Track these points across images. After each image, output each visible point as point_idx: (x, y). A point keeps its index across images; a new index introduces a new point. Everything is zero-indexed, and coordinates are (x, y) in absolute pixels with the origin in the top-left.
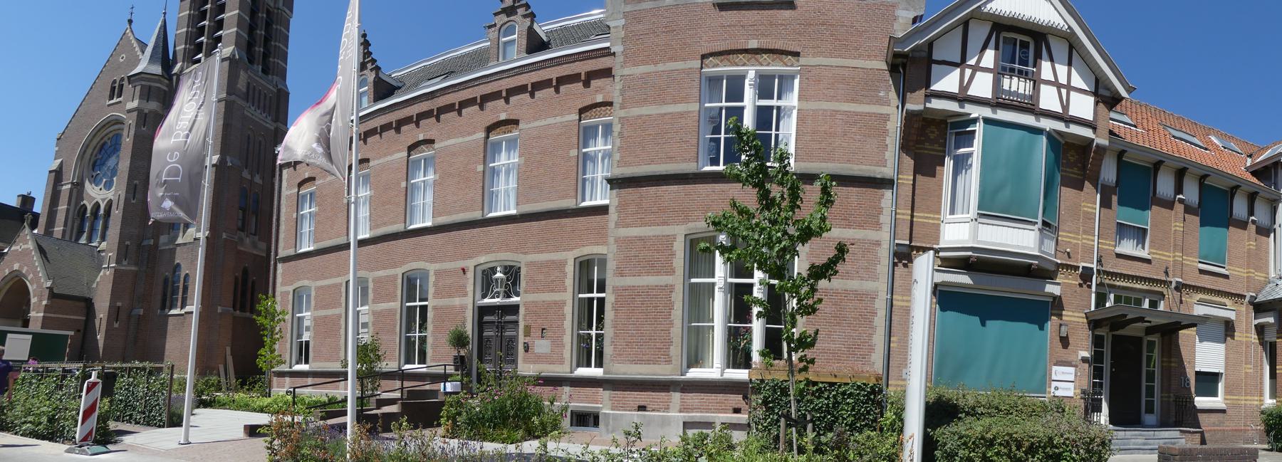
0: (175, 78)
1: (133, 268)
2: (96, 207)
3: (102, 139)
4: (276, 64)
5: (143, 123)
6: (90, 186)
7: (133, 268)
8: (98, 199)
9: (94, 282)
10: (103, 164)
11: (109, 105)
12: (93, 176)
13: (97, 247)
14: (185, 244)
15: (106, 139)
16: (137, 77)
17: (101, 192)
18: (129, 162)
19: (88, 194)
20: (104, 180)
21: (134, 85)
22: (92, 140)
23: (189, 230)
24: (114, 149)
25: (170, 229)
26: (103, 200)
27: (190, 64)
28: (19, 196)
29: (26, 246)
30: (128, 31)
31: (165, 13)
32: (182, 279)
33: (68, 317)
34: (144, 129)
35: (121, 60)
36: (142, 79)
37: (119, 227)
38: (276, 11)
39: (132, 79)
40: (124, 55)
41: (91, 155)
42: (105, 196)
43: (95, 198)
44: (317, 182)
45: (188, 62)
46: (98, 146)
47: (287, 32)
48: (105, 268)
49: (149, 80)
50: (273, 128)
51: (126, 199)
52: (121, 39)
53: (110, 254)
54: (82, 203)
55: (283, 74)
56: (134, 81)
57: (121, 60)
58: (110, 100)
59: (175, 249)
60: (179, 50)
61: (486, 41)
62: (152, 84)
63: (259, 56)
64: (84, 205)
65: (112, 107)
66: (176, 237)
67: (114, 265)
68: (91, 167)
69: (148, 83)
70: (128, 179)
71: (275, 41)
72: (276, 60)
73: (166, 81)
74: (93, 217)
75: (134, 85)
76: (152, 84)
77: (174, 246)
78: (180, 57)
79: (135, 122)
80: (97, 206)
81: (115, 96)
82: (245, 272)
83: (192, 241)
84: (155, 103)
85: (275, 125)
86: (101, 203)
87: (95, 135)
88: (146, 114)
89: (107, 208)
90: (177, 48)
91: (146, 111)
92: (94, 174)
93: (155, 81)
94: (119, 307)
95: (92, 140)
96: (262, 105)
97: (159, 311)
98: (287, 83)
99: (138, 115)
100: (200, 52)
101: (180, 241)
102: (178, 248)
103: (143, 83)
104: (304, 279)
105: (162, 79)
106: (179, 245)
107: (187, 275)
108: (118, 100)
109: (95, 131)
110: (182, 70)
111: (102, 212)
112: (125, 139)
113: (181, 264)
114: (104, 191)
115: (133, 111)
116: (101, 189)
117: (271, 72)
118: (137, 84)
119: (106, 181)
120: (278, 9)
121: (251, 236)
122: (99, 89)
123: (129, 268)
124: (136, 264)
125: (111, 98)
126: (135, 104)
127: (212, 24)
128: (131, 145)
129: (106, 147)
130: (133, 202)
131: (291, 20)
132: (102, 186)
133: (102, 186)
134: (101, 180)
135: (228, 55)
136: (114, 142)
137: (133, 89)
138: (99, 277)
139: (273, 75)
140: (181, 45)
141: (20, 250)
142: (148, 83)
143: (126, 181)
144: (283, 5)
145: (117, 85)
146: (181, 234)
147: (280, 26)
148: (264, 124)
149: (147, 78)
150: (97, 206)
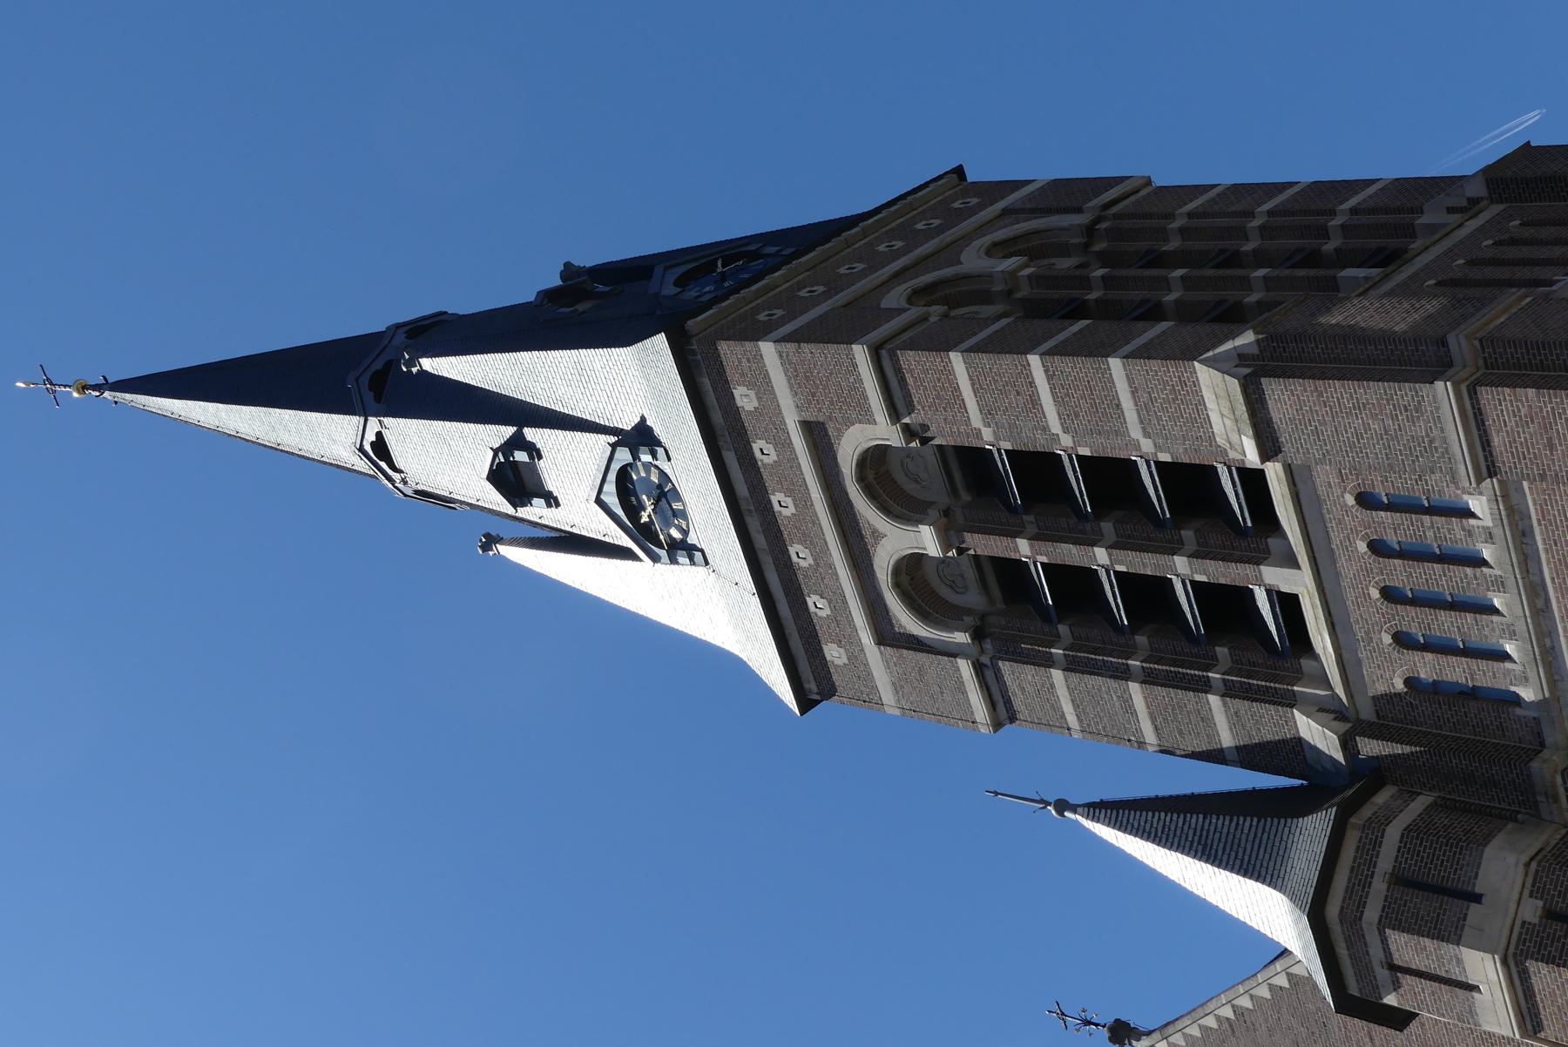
0: (1370, 747)
16: (1342, 951)
21: (1382, 974)
69: (1379, 886)
71: (1324, 234)
75: (1382, 974)
76: (1385, 863)
78: (1266, 724)
84: (1489, 851)
88: (1550, 915)
90: (1227, 739)
91: (1532, 911)
93: (1370, 848)
98: (1470, 173)
103: (1372, 914)
105: (1366, 812)
110: (1329, 711)
118: (1376, 953)
120: (1090, 230)
126: (1483, 968)
127: (1107, 527)
131: (1158, 181)
140: (1208, 720)
142: (1379, 886)
149: (1349, 891)
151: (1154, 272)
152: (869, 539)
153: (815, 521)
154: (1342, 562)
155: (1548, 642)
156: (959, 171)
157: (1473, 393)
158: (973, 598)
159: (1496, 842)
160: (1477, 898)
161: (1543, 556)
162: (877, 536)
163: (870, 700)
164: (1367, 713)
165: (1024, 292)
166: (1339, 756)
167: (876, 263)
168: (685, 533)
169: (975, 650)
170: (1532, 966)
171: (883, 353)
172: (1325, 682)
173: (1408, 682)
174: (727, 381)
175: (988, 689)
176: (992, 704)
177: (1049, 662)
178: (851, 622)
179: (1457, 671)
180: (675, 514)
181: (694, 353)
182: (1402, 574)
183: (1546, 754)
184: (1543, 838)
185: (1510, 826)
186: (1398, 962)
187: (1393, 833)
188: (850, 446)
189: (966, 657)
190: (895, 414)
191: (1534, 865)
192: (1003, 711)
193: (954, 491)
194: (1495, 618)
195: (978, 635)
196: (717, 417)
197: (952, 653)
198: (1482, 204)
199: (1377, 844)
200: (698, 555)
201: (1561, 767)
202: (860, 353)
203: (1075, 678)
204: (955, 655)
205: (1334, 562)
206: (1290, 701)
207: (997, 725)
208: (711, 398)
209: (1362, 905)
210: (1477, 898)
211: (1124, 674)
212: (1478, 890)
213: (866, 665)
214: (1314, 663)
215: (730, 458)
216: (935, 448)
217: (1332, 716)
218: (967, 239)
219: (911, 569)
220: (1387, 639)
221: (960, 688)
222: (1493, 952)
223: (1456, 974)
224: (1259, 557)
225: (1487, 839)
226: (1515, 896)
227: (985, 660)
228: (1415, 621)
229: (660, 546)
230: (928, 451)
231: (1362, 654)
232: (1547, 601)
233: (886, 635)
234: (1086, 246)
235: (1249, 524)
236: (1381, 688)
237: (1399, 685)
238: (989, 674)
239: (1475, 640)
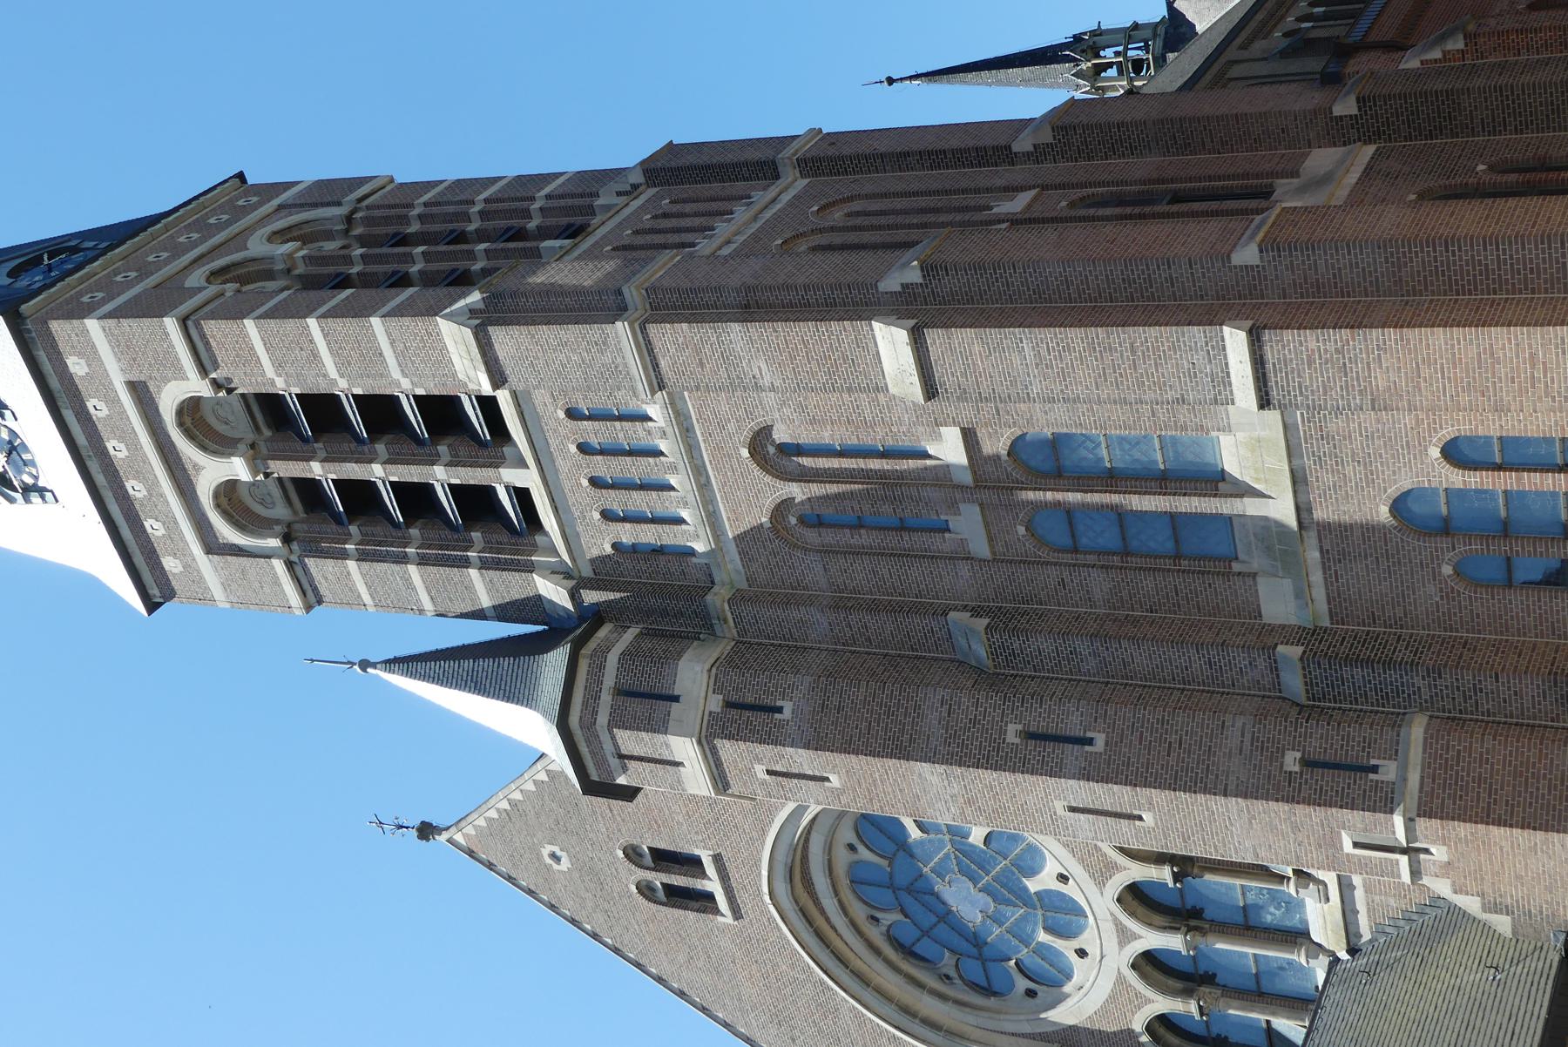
0: (591, 597)
1: (1417, 731)
2: (1149, 969)
3: (877, 951)
4: (551, 203)
5: (764, 716)
6: (1069, 1002)
7: (1417, 731)
8: (1120, 959)
9: (1486, 926)
10: (976, 941)
11: (737, 913)
12: (1031, 993)
13: (1335, 961)
14: (1298, 480)
15: (875, 934)
16: (584, 749)
17: (1093, 950)
18: (925, 768)
19: (1104, 1011)
20: (1043, 937)
21: (614, 762)
22: (880, 992)
23: (1231, 466)
24: (909, 890)
26: (1125, 937)
27: (539, 539)
30: (459, 838)
31: (365, 665)
32: (1474, 480)
35: (565, 864)
36: (589, 725)
37: (1218, 804)
39: (595, 777)
40: (546, 851)
41: (942, 997)
42: (1108, 928)
43: (1120, 980)
45: (534, 548)
46: (906, 966)
48: (1415, 873)
49: (593, 697)
51: (1086, 774)
52: (490, 866)
53: (1348, 846)
54: (1145, 1039)
56: (601, 763)
57: (565, 864)
58: (717, 911)
59: (1325, 529)
60: (490, 589)
64: (1149, 1029)
65: (742, 898)
66: (1268, 530)
67: (1398, 820)
68: (992, 1002)
69: (606, 698)
70: (996, 767)
71: (527, 214)
73: (603, 632)
74: (1204, 989)
75: (614, 762)
76: (609, 681)
77: (1312, 538)
78: (514, 586)
79: (760, 749)
80: (1151, 965)
83: (1273, 417)
87: (857, 975)
88: (729, 705)
89: (1158, 919)
91: (716, 703)
92: (1022, 984)
95: (880, 992)
96: (697, 221)
99: (730, 737)
100: (488, 493)
101: (1282, 509)
102: (1319, 514)
103: (603, 719)
105: (592, 644)
106: (1302, 509)
107: (1454, 453)
108: (710, 869)
109: (867, 995)
110: (561, 573)
111: (1173, 942)
112: (759, 761)
113: (1393, 492)
114: (1087, 940)
115: (718, 763)
116: (1082, 953)
118: (608, 747)
119: (1047, 929)
120: (349, 219)
122: (681, 958)
123: (1416, 754)
124: (1398, 721)
126: (684, 748)
127: (380, 448)
128: (854, 760)
129: (908, 934)
130: (1100, 740)
131: (399, 179)
132: (1066, 947)
133: (1066, 947)
134: (1042, 951)
135: (468, 333)
136: (887, 896)
137: (632, 764)
140: (470, 588)
143: (1006, 778)
144: (339, 204)
145: (658, 879)
146: (1251, 507)
147: (411, 206)
148: (778, 206)
149: (585, 704)
150: (1151, 965)
152: (191, 471)
153: (145, 460)
154: (560, 462)
155: (711, 507)
156: (241, 176)
157: (643, 329)
158: (281, 511)
159: (686, 656)
160: (676, 699)
161: (702, 445)
162: (197, 468)
163: (206, 599)
164: (587, 572)
165: (300, 269)
166: (569, 606)
167: (178, 251)
168: (36, 478)
169: (285, 551)
170: (718, 742)
171: (190, 323)
172: (554, 551)
173: (614, 546)
174: (59, 353)
175: (298, 581)
176: (303, 593)
177: (344, 555)
178: (183, 538)
179: (648, 535)
180: (25, 463)
181: (29, 331)
182: (604, 467)
183: (716, 589)
184: (719, 650)
185: (696, 643)
186: (624, 752)
187: (612, 659)
188: (168, 401)
189: (279, 557)
190: (203, 371)
191: (714, 670)
192: (311, 596)
193: (257, 429)
194: (672, 493)
195: (287, 539)
196: (54, 383)
197: (267, 555)
198: (641, 189)
199: (602, 667)
200: (48, 495)
201: (727, 598)
202: (171, 324)
203: (366, 565)
204: (269, 557)
205: (554, 462)
206: (530, 568)
207: (309, 608)
208: (47, 367)
209: (595, 713)
210: (676, 699)
211: (403, 559)
212: (676, 693)
213: (199, 571)
214: (545, 538)
215: (69, 416)
216: (255, 409)
217: (562, 576)
218: (250, 230)
219: (228, 494)
220: (597, 516)
221: (276, 582)
222: (691, 736)
223: (667, 756)
224: (497, 462)
225: (680, 655)
226: (703, 694)
227: (294, 558)
228: (616, 501)
229: (15, 490)
230: (233, 398)
231: (580, 529)
232: (708, 477)
233: (213, 546)
234: (347, 231)
235: (488, 438)
236: (595, 553)
237: (609, 550)
238: (298, 569)
239: (660, 511)
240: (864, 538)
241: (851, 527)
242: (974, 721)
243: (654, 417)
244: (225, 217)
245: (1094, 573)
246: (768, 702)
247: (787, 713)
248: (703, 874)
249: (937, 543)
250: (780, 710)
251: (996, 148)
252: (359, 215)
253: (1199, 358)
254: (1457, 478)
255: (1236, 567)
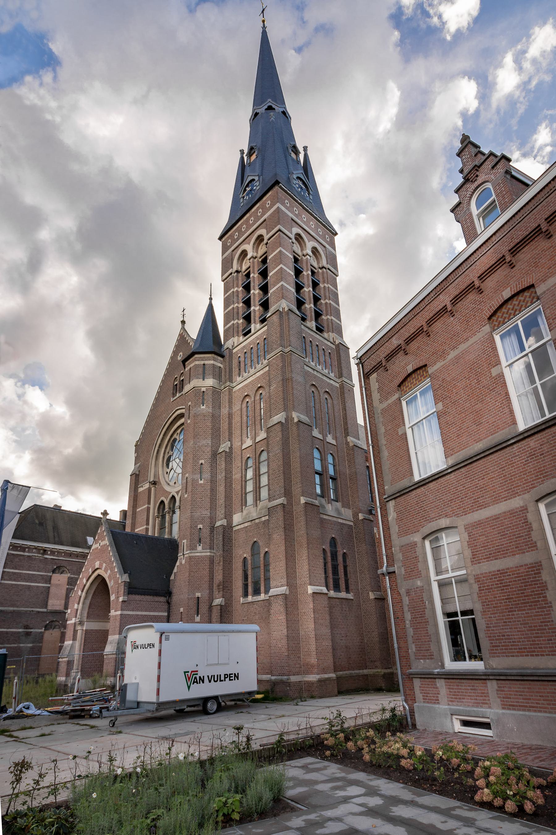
25: (242, 506)
28: (121, 511)
29: (102, 543)
33: (21, 572)
34: (204, 407)
38: (320, 271)
43: (170, 493)
44: (431, 370)
47: (337, 306)
50: (337, 385)
55: (339, 331)
58: (173, 397)
61: (424, 547)
62: (206, 362)
63: (311, 312)
68: (165, 465)
69: (202, 362)
71: (327, 315)
72: (328, 317)
76: (206, 362)
81: (178, 392)
82: (333, 542)
85: (339, 381)
86: (176, 496)
91: (203, 389)
94: (198, 598)
97: (241, 598)
98: (344, 339)
104: (439, 517)
108: (180, 394)
117: (326, 329)
121: (333, 502)
125: (174, 395)
130: (202, 482)
138: (176, 567)
139: (328, 332)
141: (99, 547)
151: (314, 318)
162: (249, 243)
209: (198, 360)
210: (204, 380)
240: (245, 418)
241: (247, 415)
242: (204, 452)
243: (528, 342)
244: (321, 233)
245: (240, 474)
246: (205, 402)
247: (202, 407)
248: (180, 392)
249: (244, 436)
250: (203, 405)
251: (348, 433)
252: (324, 270)
253: (278, 493)
254: (262, 555)
255: (244, 507)
